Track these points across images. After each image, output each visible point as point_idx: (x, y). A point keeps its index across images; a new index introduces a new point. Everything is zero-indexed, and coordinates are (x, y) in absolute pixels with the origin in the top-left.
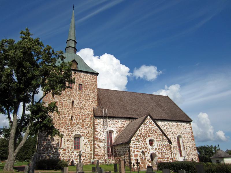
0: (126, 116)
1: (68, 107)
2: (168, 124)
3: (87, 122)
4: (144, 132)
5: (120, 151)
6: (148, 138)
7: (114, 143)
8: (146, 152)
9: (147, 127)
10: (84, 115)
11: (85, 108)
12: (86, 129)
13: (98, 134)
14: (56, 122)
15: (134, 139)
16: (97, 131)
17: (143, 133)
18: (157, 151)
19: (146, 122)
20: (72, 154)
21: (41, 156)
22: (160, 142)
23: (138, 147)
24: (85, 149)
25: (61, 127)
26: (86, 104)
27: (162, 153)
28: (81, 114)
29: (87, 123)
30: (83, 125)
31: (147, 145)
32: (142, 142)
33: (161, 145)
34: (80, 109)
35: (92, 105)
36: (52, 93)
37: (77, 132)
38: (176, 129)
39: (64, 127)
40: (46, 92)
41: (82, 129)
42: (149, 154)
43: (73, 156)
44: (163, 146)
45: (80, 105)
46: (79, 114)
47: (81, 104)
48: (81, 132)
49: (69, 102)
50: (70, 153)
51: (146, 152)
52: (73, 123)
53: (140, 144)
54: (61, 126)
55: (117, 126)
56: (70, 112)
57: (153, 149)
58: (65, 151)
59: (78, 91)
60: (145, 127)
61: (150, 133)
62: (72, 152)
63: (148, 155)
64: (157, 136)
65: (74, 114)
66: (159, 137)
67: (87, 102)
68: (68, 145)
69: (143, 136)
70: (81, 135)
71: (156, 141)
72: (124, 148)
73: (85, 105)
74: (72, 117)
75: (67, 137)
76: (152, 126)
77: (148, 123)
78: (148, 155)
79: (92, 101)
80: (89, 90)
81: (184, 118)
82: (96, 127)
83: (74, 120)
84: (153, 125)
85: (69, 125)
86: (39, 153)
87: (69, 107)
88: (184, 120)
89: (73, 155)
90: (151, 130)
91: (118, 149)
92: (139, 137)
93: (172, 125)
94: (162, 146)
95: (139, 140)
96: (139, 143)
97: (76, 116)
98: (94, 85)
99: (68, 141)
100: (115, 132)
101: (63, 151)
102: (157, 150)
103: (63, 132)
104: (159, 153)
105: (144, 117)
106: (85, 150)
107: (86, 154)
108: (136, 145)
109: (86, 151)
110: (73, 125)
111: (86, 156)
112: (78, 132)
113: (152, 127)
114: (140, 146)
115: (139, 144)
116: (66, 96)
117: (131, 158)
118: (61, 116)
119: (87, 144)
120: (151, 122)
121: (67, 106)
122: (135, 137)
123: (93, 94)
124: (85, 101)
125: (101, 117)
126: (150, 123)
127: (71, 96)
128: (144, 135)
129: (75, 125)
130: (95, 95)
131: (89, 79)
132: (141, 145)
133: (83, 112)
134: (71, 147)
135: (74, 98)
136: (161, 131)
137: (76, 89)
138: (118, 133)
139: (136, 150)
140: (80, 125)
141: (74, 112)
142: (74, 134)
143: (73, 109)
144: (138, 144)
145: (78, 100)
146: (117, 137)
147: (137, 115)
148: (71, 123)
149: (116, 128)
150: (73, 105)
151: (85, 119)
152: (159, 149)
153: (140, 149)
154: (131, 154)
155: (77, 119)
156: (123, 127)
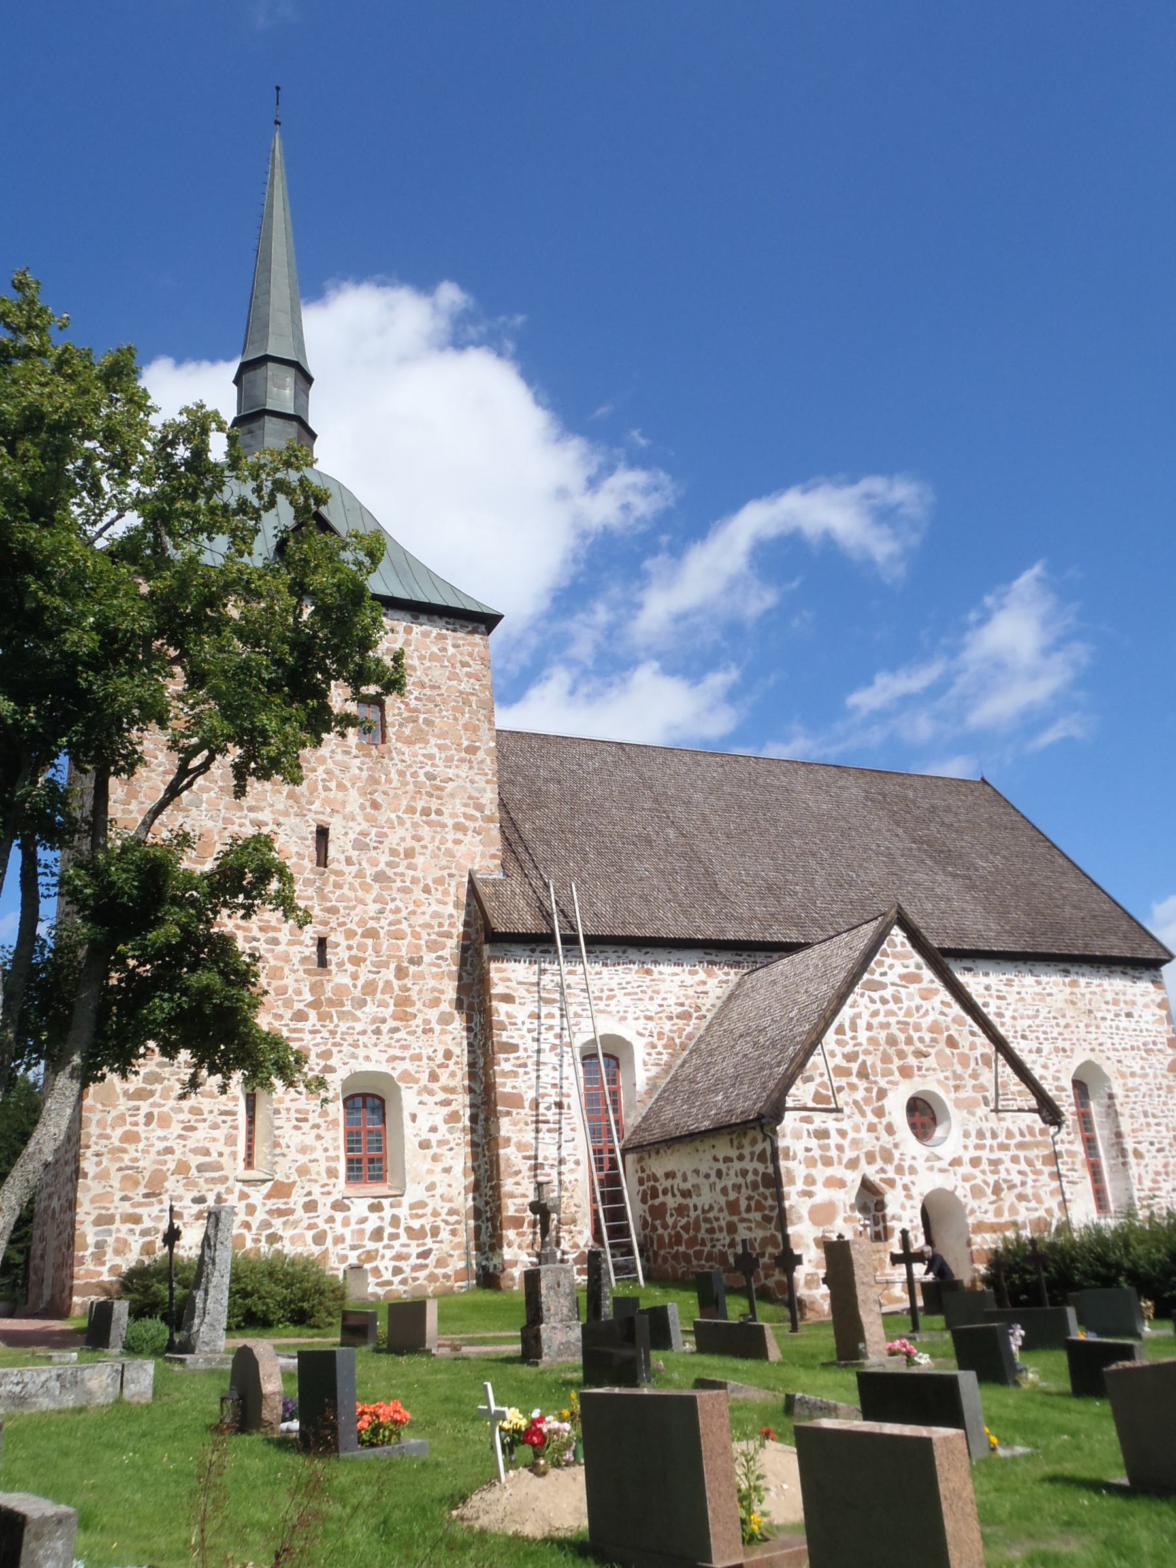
0: (709, 931)
2: (1009, 983)
3: (432, 983)
4: (872, 1041)
5: (696, 1187)
7: (638, 1129)
9: (892, 1006)
10: (404, 926)
11: (415, 881)
12: (425, 1032)
13: (521, 1070)
15: (801, 1093)
16: (514, 1048)
17: (867, 1052)
18: (965, 1179)
19: (884, 974)
20: (339, 1216)
21: (111, 1240)
22: (982, 1110)
23: (833, 1153)
24: (429, 1179)
26: (418, 849)
27: (997, 1190)
28: (384, 923)
29: (434, 990)
30: (403, 1001)
31: (897, 1138)
32: (863, 1114)
33: (988, 1134)
34: (376, 886)
35: (459, 850)
36: (235, 766)
37: (367, 1058)
38: (1062, 1022)
40: (194, 751)
41: (402, 1034)
42: (909, 1197)
43: (347, 1233)
44: (1002, 1138)
45: (373, 853)
46: (371, 924)
47: (385, 847)
50: (324, 1210)
51: (891, 1183)
52: (328, 987)
53: (852, 1128)
55: (653, 1008)
57: (938, 1164)
58: (289, 1196)
59: (354, 752)
60: (873, 1007)
61: (909, 1049)
62: (338, 1206)
63: (903, 1207)
64: (959, 1069)
65: (333, 924)
66: (975, 1075)
67: (425, 831)
68: (303, 1150)
69: (863, 1074)
70: (395, 1074)
71: (958, 1104)
72: (727, 1160)
73: (410, 854)
76: (924, 998)
77: (893, 977)
78: (903, 1207)
79: (458, 827)
81: (1114, 940)
82: (503, 1017)
83: (340, 965)
84: (926, 995)
85: (301, 1006)
86: (95, 1213)
88: (1115, 953)
89: (346, 1223)
90: (917, 1028)
91: (670, 1175)
92: (838, 1082)
93: (1038, 989)
94: (995, 1143)
95: (840, 1104)
96: (839, 1125)
97: (350, 934)
100: (640, 1053)
101: (268, 1196)
102: (966, 1169)
104: (977, 1192)
105: (869, 930)
106: (431, 1187)
107: (435, 1214)
108: (823, 1134)
109: (439, 1191)
110: (331, 1002)
111: (435, 1232)
112: (373, 1053)
113: (926, 1005)
114: (846, 1143)
115: (842, 1133)
117: (790, 1230)
119: (441, 1143)
120: (912, 969)
122: (809, 1079)
123: (464, 771)
124: (408, 825)
125: (537, 943)
128: (873, 1066)
129: (348, 1008)
132: (851, 1135)
133: (397, 910)
134: (323, 1166)
135: (327, 802)
136: (985, 1032)
138: (665, 1057)
139: (821, 1173)
140: (386, 1006)
141: (333, 911)
142: (343, 1073)
144: (833, 1133)
145: (360, 818)
146: (652, 1084)
147: (792, 921)
148: (315, 988)
149: (649, 1018)
150: (322, 860)
151: (416, 961)
152: (975, 1162)
154: (787, 1204)
155: (356, 961)
156: (698, 1008)
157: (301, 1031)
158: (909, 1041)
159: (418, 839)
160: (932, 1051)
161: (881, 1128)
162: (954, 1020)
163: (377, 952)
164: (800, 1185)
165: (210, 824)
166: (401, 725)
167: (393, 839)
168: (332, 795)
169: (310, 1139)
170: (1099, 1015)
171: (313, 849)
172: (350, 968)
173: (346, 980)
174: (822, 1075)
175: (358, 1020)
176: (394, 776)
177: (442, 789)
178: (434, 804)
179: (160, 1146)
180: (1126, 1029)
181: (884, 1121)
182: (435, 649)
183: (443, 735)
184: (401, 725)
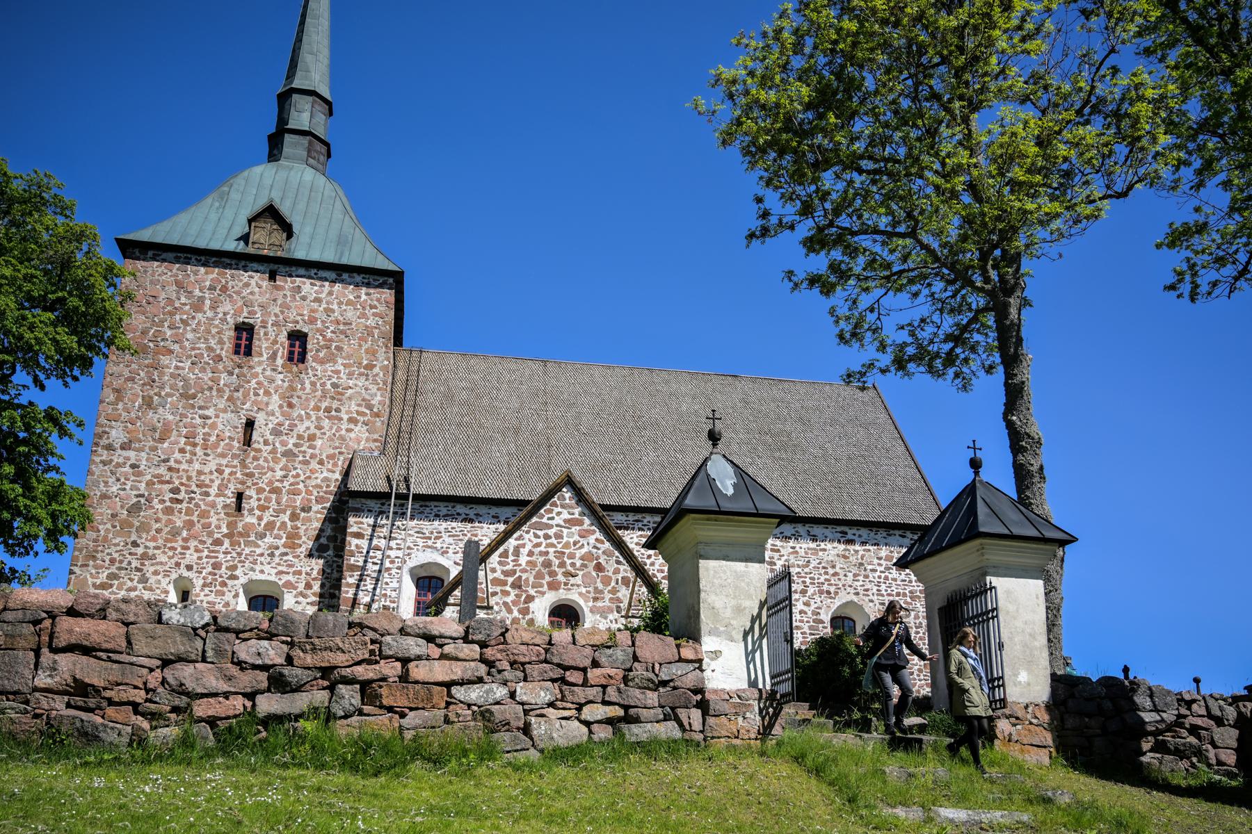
1: (219, 450)
6: (543, 593)
9: (553, 540)
10: (301, 486)
19: (552, 518)
25: (181, 543)
28: (286, 484)
37: (262, 572)
38: (831, 571)
39: (196, 543)
41: (290, 557)
45: (285, 438)
46: (277, 484)
47: (295, 434)
48: (280, 568)
49: (228, 425)
52: (240, 525)
54: (179, 538)
56: (231, 474)
59: (280, 369)
60: (536, 541)
64: (600, 586)
65: (249, 484)
66: (614, 591)
67: (326, 423)
69: (517, 585)
70: (280, 583)
73: (312, 438)
74: (240, 496)
75: (207, 589)
79: (351, 420)
80: (340, 361)
82: (353, 548)
83: (251, 511)
87: (230, 447)
90: (572, 556)
98: (371, 334)
103: (189, 568)
110: (241, 535)
112: (267, 568)
113: (582, 541)
116: (214, 393)
118: (183, 493)
121: (216, 446)
126: (571, 523)
127: (240, 394)
128: (527, 579)
130: (374, 389)
131: (349, 303)
137: (273, 357)
141: (251, 475)
143: (250, 460)
148: (231, 525)
150: (248, 442)
151: (306, 509)
157: (218, 552)
158: (562, 565)
160: (581, 573)
163: (278, 503)
165: (171, 417)
166: (318, 351)
167: (301, 428)
168: (259, 398)
170: (870, 567)
171: (241, 435)
172: (257, 512)
173: (254, 521)
175: (259, 546)
176: (308, 385)
177: (342, 394)
178: (335, 405)
180: (895, 580)
181: (527, 617)
182: (351, 297)
183: (349, 357)
184: (318, 351)
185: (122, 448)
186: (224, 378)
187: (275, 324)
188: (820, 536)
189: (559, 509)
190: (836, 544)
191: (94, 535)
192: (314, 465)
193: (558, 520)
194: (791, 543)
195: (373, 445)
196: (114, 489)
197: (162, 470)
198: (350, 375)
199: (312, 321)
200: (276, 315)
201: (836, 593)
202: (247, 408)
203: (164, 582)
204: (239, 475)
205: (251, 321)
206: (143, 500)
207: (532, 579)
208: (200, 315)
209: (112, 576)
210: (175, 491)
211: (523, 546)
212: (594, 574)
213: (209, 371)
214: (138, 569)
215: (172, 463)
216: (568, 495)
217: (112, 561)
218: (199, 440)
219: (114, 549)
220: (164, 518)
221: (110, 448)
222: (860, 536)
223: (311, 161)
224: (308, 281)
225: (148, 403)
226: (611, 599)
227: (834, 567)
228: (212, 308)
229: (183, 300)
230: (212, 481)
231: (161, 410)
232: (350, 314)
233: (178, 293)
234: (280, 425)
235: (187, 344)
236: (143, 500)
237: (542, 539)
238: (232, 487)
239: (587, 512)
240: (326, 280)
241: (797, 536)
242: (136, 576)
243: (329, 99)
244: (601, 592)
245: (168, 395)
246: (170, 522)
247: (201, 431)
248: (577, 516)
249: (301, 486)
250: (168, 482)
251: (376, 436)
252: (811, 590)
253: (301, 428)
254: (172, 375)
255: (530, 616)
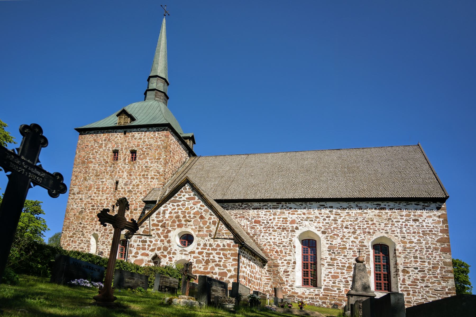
4: (171, 217)
6: (175, 229)
8: (165, 256)
9: (181, 207)
14: (88, 216)
19: (181, 198)
23: (147, 247)
38: (370, 223)
47: (132, 185)
60: (173, 207)
64: (202, 225)
66: (208, 227)
67: (143, 180)
69: (163, 226)
76: (194, 205)
79: (152, 178)
90: (189, 213)
99: (104, 245)
103: (97, 230)
116: (105, 174)
121: (106, 191)
122: (143, 227)
123: (156, 164)
126: (189, 199)
127: (114, 173)
130: (160, 166)
131: (152, 138)
132: (154, 242)
139: (141, 252)
144: (148, 242)
152: (200, 253)
153: (150, 251)
158: (185, 217)
159: (140, 182)
160: (193, 220)
161: (165, 241)
162: (204, 211)
164: (133, 254)
165: (92, 183)
166: (140, 156)
167: (134, 182)
169: (105, 247)
174: (147, 226)
176: (137, 168)
179: (74, 247)
181: (167, 239)
183: (151, 156)
185: (77, 194)
186: (109, 169)
187: (126, 149)
188: (364, 207)
189: (184, 194)
190: (373, 210)
191: (69, 221)
192: (138, 194)
193: (184, 198)
194: (347, 211)
195: (160, 186)
196: (75, 207)
197: (89, 200)
198: (152, 163)
199: (138, 146)
200: (126, 146)
201: (374, 233)
202: (116, 178)
203: (89, 235)
204: (113, 200)
205: (118, 149)
206: (83, 210)
207: (170, 224)
208: (101, 149)
209: (74, 234)
210: (93, 206)
211: (167, 210)
212: (199, 220)
213: (104, 166)
214: (81, 231)
215: (92, 197)
216: (188, 188)
217: (74, 229)
218: (101, 189)
219: (74, 225)
220: (89, 215)
221: (74, 194)
222: (389, 206)
223: (156, 99)
224: (137, 133)
225: (85, 179)
226: (207, 231)
227: (372, 221)
228: (105, 146)
229: (96, 145)
230: (105, 202)
231: (89, 181)
232: (152, 142)
233: (94, 143)
234: (127, 182)
235: (97, 159)
236: (83, 210)
237: (176, 207)
238: (111, 204)
239: (196, 194)
240: (143, 131)
241: (350, 208)
242: (81, 233)
243: (164, 77)
244: (202, 228)
245: (91, 176)
246: (91, 216)
247: (101, 186)
248: (192, 196)
249: (134, 202)
250: (91, 203)
251: (161, 183)
252: (358, 232)
253: (134, 182)
254: (93, 170)
255: (169, 239)
